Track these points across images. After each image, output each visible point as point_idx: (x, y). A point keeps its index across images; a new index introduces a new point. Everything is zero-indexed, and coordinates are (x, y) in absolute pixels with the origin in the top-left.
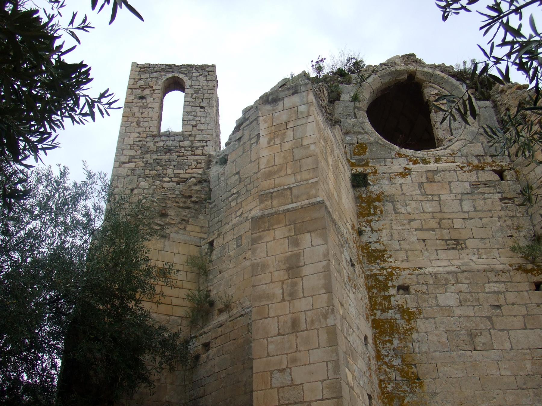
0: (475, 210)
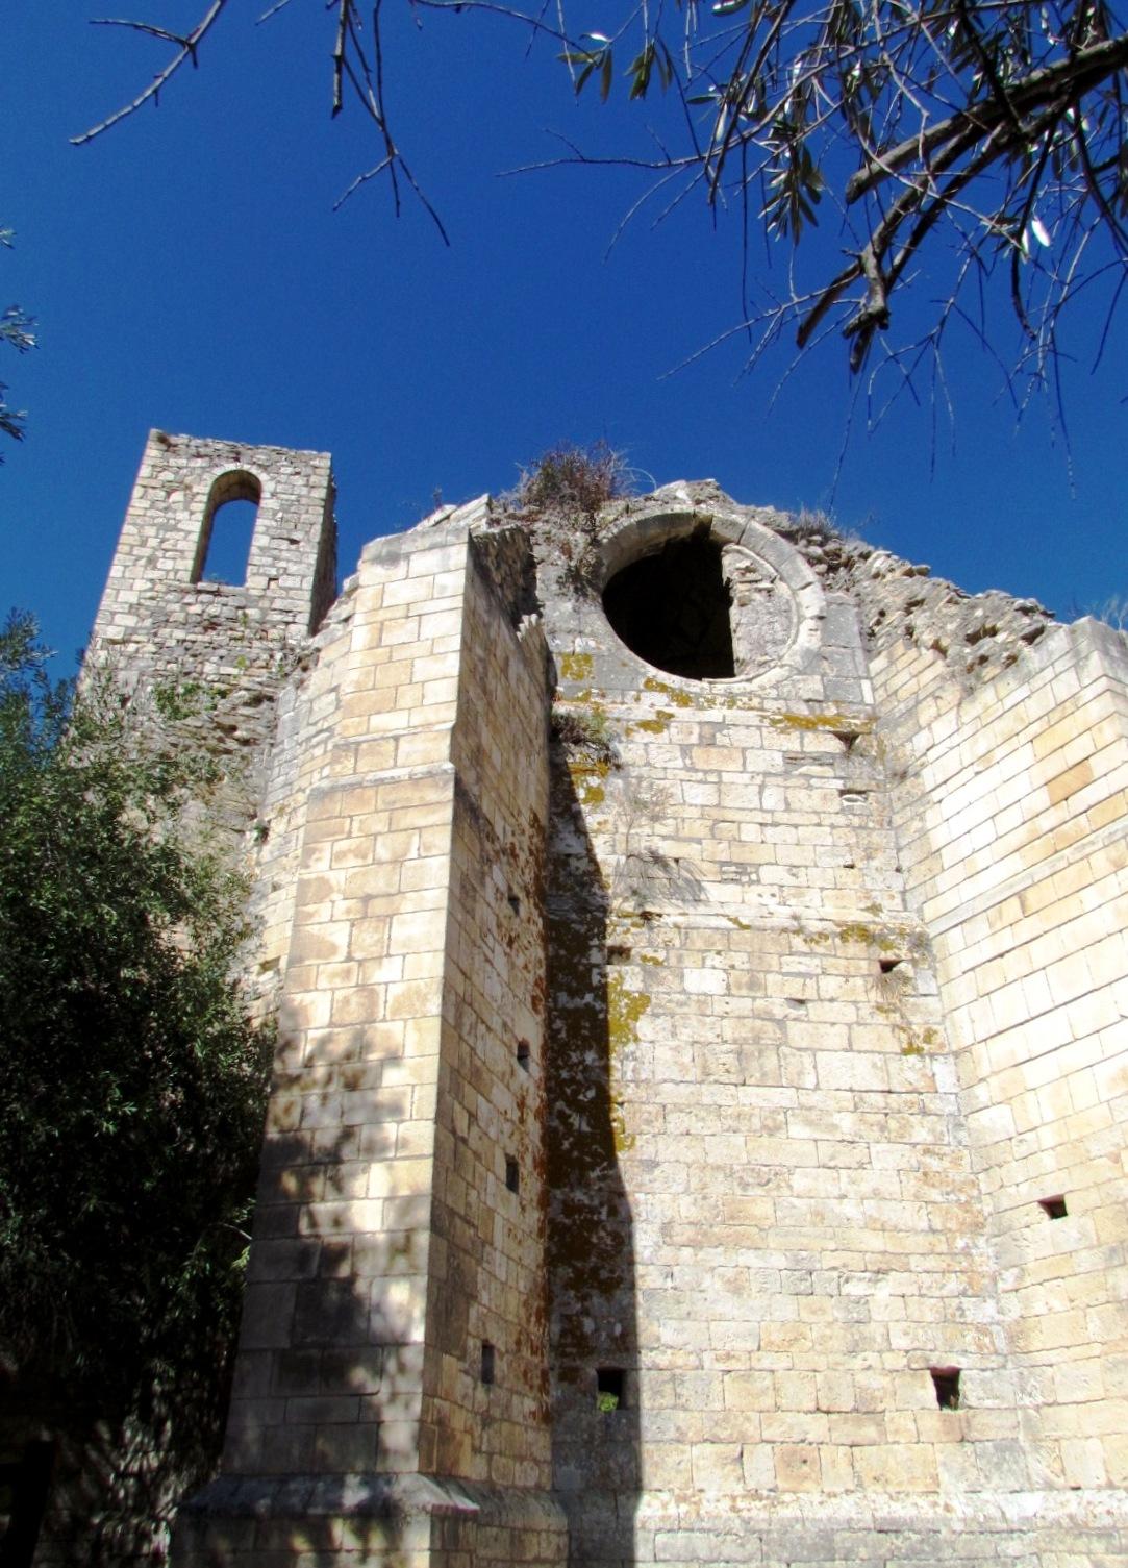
0: (788, 808)
